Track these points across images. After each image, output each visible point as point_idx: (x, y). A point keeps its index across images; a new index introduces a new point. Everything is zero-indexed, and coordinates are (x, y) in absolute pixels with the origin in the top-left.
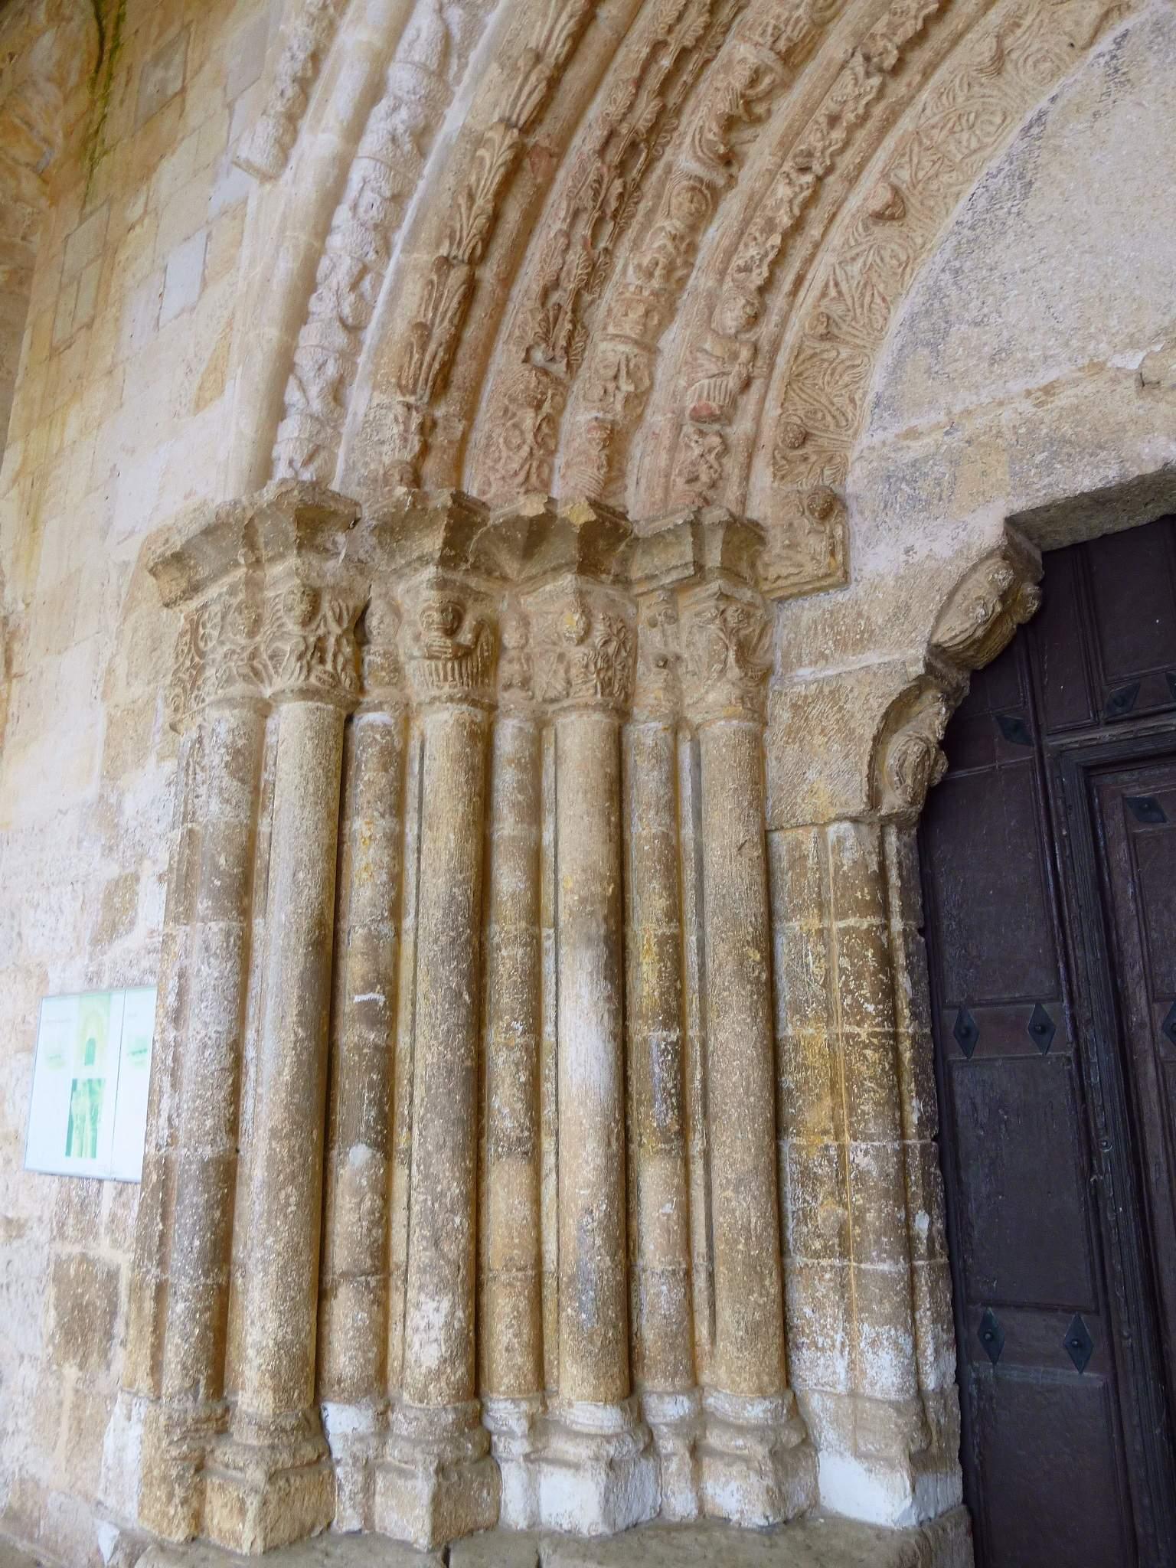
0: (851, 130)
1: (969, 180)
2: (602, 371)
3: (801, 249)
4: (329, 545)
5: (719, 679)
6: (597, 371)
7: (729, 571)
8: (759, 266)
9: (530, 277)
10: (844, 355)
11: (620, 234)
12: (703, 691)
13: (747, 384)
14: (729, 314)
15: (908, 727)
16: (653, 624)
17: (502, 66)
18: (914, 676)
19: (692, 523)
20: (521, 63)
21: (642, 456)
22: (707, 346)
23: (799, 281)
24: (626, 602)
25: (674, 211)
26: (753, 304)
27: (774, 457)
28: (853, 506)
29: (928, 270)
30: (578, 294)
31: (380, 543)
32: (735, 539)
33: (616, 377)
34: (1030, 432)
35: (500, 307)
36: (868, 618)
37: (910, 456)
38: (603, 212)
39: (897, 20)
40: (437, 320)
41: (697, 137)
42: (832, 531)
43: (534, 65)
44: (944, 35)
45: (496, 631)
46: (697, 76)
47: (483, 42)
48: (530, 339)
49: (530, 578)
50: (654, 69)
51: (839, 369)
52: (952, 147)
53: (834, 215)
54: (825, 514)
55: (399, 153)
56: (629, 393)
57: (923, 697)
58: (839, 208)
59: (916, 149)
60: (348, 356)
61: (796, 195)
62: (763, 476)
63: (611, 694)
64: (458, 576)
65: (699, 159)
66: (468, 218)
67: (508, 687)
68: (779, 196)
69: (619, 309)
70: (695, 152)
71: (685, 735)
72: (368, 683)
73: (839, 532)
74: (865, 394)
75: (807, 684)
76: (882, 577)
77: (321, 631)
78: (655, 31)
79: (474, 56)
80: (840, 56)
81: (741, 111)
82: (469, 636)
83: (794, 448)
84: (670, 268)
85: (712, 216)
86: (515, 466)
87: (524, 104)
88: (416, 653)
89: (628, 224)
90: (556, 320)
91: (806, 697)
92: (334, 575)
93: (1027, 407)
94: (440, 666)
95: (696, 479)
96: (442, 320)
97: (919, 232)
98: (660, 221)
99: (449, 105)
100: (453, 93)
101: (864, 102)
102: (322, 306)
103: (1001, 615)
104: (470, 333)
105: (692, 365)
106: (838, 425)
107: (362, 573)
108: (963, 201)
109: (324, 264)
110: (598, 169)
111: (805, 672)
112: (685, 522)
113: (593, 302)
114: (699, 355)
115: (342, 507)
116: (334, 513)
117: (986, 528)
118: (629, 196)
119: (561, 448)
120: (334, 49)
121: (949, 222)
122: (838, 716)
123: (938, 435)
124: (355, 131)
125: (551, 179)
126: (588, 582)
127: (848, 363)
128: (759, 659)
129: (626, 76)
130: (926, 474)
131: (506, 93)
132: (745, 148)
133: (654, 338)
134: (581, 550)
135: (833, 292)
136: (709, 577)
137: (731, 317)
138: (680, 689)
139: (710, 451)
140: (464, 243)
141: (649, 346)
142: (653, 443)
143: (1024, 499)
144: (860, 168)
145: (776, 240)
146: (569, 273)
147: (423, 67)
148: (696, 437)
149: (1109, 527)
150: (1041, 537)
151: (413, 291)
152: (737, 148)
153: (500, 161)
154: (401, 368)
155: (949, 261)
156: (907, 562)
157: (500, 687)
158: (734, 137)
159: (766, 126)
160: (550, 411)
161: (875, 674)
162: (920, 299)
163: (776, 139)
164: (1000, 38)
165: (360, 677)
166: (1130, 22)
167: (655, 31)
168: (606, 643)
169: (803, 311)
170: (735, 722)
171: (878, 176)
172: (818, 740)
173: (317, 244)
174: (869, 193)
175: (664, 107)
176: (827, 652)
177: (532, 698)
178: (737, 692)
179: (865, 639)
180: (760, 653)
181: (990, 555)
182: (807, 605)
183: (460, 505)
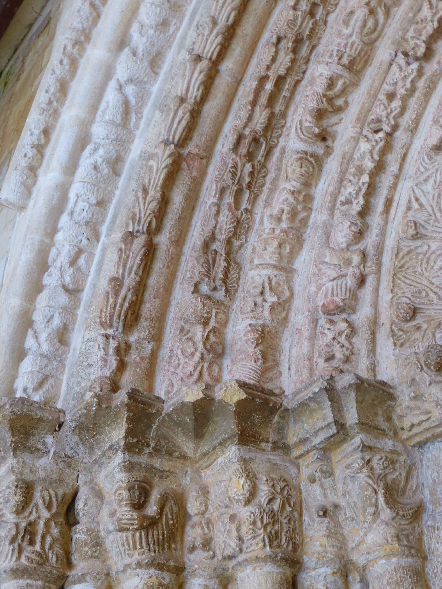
0: (405, 99)
2: (252, 291)
3: (385, 181)
4: (40, 446)
5: (374, 520)
6: (248, 291)
7: (366, 425)
8: (356, 198)
9: (195, 237)
12: (361, 533)
13: (362, 281)
14: (339, 234)
17: (162, 111)
19: (326, 389)
20: (172, 106)
22: (327, 259)
23: (389, 202)
25: (290, 176)
26: (356, 224)
27: (392, 331)
30: (229, 242)
31: (81, 439)
32: (367, 398)
33: (262, 293)
35: (175, 260)
38: (241, 185)
39: (420, 26)
40: (127, 273)
41: (299, 127)
43: (181, 104)
45: (180, 501)
48: (196, 279)
49: (205, 455)
51: (433, 257)
55: (99, 175)
56: (273, 303)
58: (408, 149)
60: (70, 311)
61: (374, 147)
62: (386, 348)
63: (279, 546)
64: (143, 459)
65: (302, 140)
66: (144, 205)
67: (193, 549)
68: (362, 150)
69: (259, 247)
70: (298, 136)
72: (75, 558)
77: (32, 518)
78: (260, 71)
79: (146, 111)
81: (325, 105)
82: (155, 508)
83: (407, 321)
84: (293, 214)
86: (190, 368)
87: (177, 129)
88: (111, 528)
89: (261, 191)
92: (45, 470)
94: (130, 538)
96: (130, 273)
101: (410, 80)
102: (51, 280)
104: (153, 280)
105: (319, 274)
107: (69, 465)
109: (54, 251)
110: (233, 159)
112: (321, 389)
113: (241, 246)
114: (321, 266)
115: (47, 415)
116: (41, 420)
118: (258, 173)
120: (58, 126)
124: (71, 168)
125: (203, 173)
126: (250, 451)
128: (409, 499)
132: (335, 128)
133: (289, 262)
134: (238, 424)
135: (415, 205)
136: (352, 433)
137: (342, 235)
138: (342, 535)
139: (340, 334)
140: (143, 220)
141: (285, 267)
142: (296, 337)
144: (417, 121)
145: (365, 178)
146: (220, 229)
148: (328, 326)
151: (112, 257)
152: (329, 129)
153: (163, 166)
154: (102, 310)
157: (186, 551)
158: (325, 123)
159: (347, 112)
165: (68, 554)
167: (260, 71)
168: (270, 501)
169: (396, 222)
170: (394, 560)
171: (431, 123)
173: (47, 241)
177: (214, 556)
178: (392, 531)
180: (409, 493)
183: (136, 400)
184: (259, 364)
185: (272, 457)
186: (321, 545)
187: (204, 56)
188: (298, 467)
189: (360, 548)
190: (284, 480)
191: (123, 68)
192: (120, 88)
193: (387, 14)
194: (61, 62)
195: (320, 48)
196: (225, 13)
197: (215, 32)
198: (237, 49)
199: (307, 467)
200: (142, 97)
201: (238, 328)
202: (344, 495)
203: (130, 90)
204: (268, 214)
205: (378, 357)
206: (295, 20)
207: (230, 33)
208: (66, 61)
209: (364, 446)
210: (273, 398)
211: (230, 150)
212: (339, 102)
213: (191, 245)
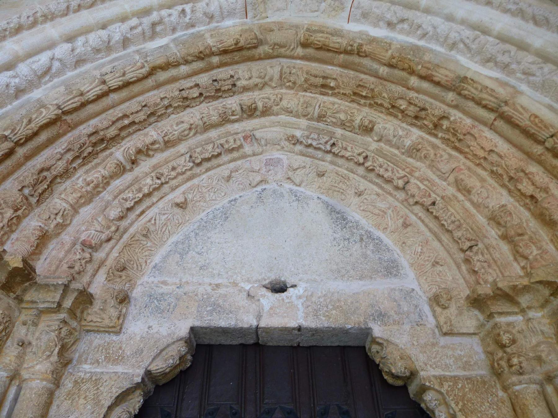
0: (179, 174)
1: (208, 208)
2: (51, 209)
5: (46, 359)
6: (49, 208)
7: (72, 312)
9: (39, 161)
10: (148, 245)
11: (83, 165)
12: (35, 363)
13: (109, 240)
15: (124, 404)
16: (24, 324)
18: (136, 382)
19: (65, 285)
20: (74, 92)
21: (53, 250)
22: (100, 219)
23: (143, 212)
24: (16, 309)
25: (107, 168)
28: (133, 302)
29: (186, 229)
30: (56, 177)
33: (56, 214)
34: (208, 298)
35: (19, 165)
36: (124, 351)
37: (161, 291)
41: (126, 149)
42: (121, 309)
43: (79, 96)
44: (216, 162)
46: (135, 132)
47: (62, 78)
48: (26, 183)
50: (120, 122)
52: (207, 195)
53: (163, 197)
54: (121, 302)
56: (59, 223)
57: (135, 393)
58: (165, 196)
59: (196, 190)
62: (101, 277)
65: (124, 156)
66: (24, 128)
69: (69, 190)
71: (16, 382)
73: (124, 310)
74: (151, 262)
75: (86, 373)
76: (135, 335)
79: (56, 80)
80: (183, 151)
83: (118, 271)
84: (97, 186)
85: (120, 177)
87: (69, 105)
89: (87, 164)
90: (41, 182)
91: (83, 379)
93: (209, 289)
95: (73, 268)
97: (188, 216)
98: (100, 169)
99: (37, 89)
100: (41, 87)
101: (186, 168)
103: (179, 364)
106: (137, 269)
108: (205, 213)
111: (87, 367)
113: (60, 183)
114: (95, 221)
117: (183, 330)
119: (17, 231)
121: (199, 217)
122: (95, 392)
123: (174, 287)
125: (64, 134)
127: (149, 248)
129: (109, 118)
130: (165, 300)
131: (63, 98)
132: (141, 162)
135: (153, 222)
136: (62, 311)
137: (113, 213)
138: (24, 359)
139: (84, 259)
140: (18, 135)
141: (75, 209)
142: (60, 246)
143: (200, 322)
144: (177, 187)
145: (141, 195)
146: (56, 168)
147: (35, 72)
148: (80, 251)
149: (223, 342)
150: (199, 338)
152: (138, 160)
153: (49, 117)
155: (195, 229)
156: (147, 332)
158: (139, 156)
160: (21, 215)
161: (119, 377)
162: (182, 237)
163: (152, 164)
164: (231, 172)
166: (267, 186)
169: (140, 223)
170: (44, 383)
172: (82, 401)
174: (177, 196)
175: (119, 135)
176: (100, 360)
178: (52, 368)
179: (119, 359)
180: (69, 352)
181: (181, 339)
182: (98, 337)
184: (32, 249)
185: (11, 302)
186: (10, 360)
187: (108, 84)
188: (20, 313)
189: (30, 369)
190: (10, 317)
191: (62, 50)
192: (52, 59)
193: (195, 134)
194: (28, 17)
195: (159, 124)
196: (131, 75)
197: (121, 79)
198: (124, 93)
199: (26, 315)
200: (59, 73)
201: (31, 223)
202: (37, 339)
203: (56, 65)
204: (84, 177)
205: (94, 280)
206: (158, 104)
207: (127, 84)
208: (31, 19)
209: (64, 320)
210: (33, 274)
211: (87, 134)
212: (151, 153)
213: (33, 164)
